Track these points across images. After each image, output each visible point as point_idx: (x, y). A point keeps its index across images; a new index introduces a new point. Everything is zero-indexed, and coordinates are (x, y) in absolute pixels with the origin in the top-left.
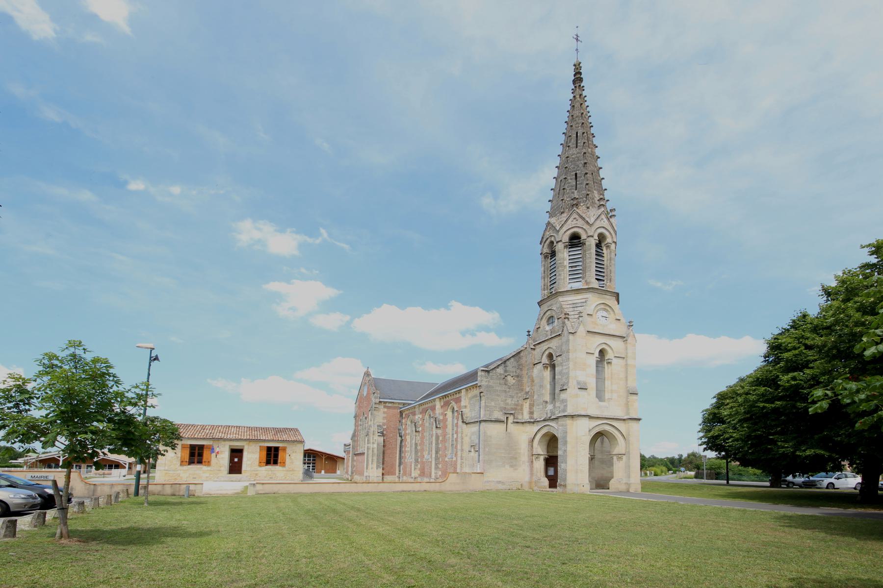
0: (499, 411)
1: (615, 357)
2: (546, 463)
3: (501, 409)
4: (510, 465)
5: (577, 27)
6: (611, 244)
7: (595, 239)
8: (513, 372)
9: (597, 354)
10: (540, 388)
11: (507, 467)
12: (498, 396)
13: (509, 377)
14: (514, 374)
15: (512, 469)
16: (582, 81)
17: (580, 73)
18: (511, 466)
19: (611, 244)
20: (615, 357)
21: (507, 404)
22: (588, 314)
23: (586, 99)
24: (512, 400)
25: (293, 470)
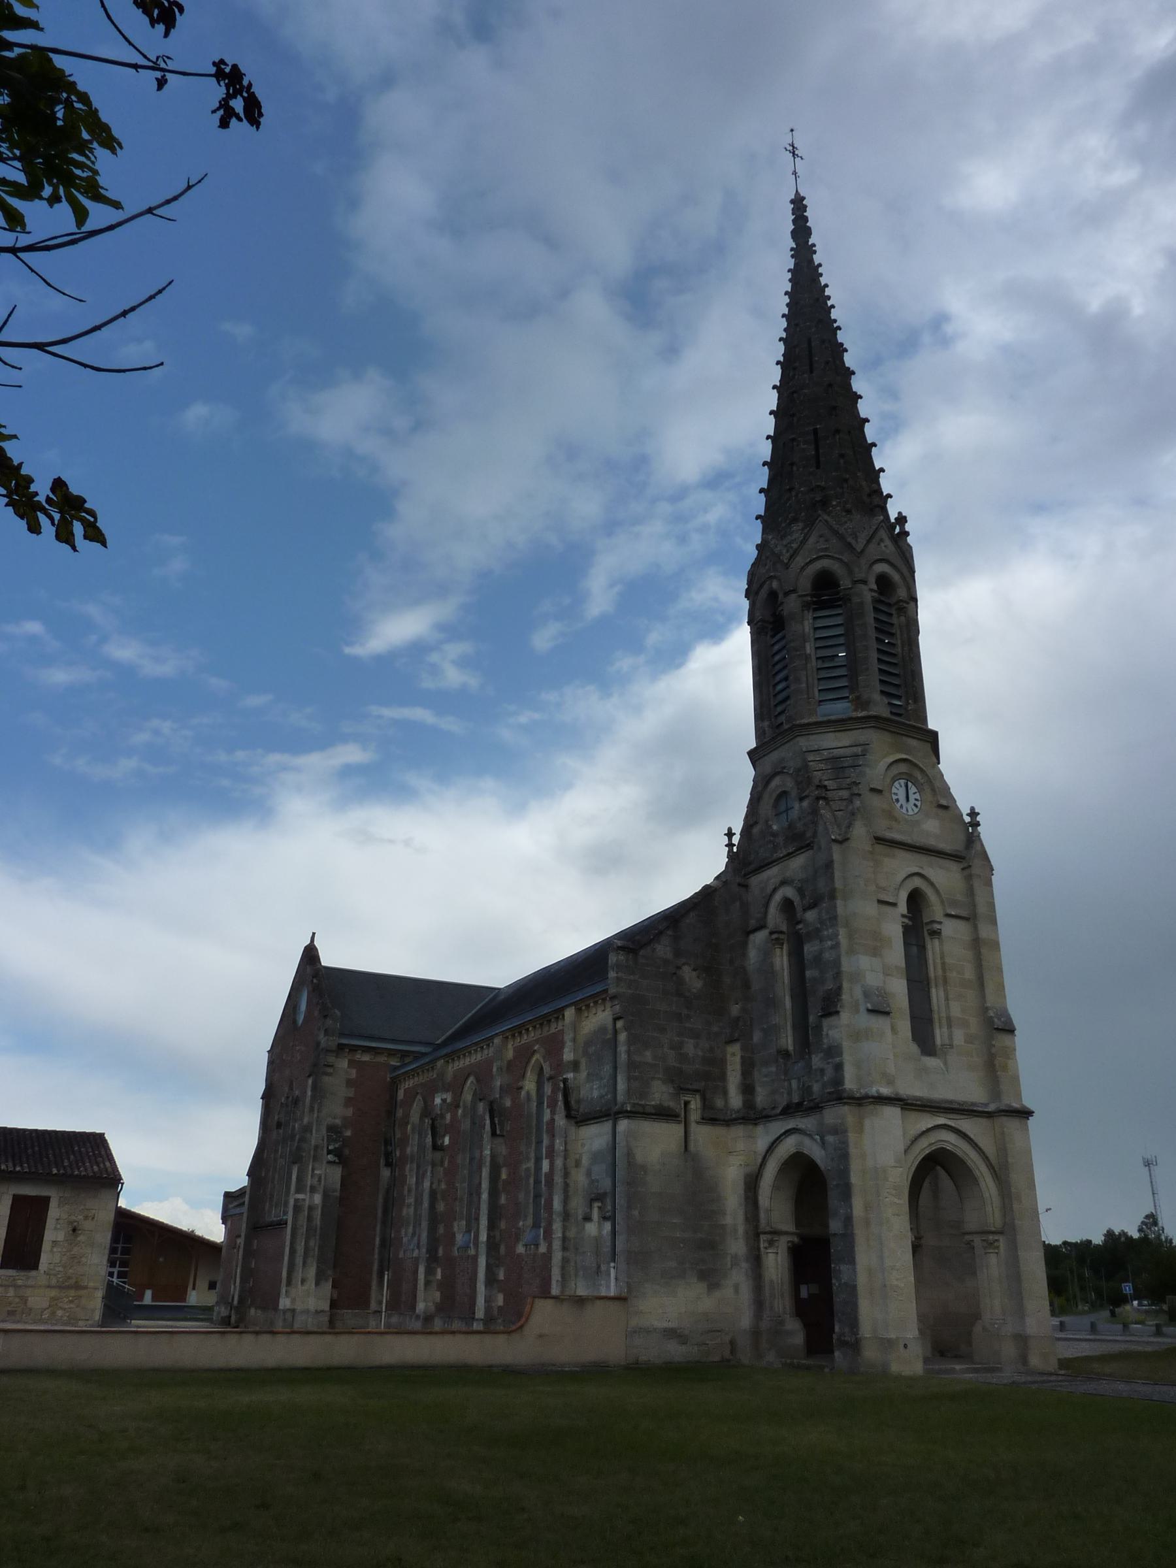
5: (792, 130)
7: (800, 596)
9: (903, 908)
25: (77, 1287)
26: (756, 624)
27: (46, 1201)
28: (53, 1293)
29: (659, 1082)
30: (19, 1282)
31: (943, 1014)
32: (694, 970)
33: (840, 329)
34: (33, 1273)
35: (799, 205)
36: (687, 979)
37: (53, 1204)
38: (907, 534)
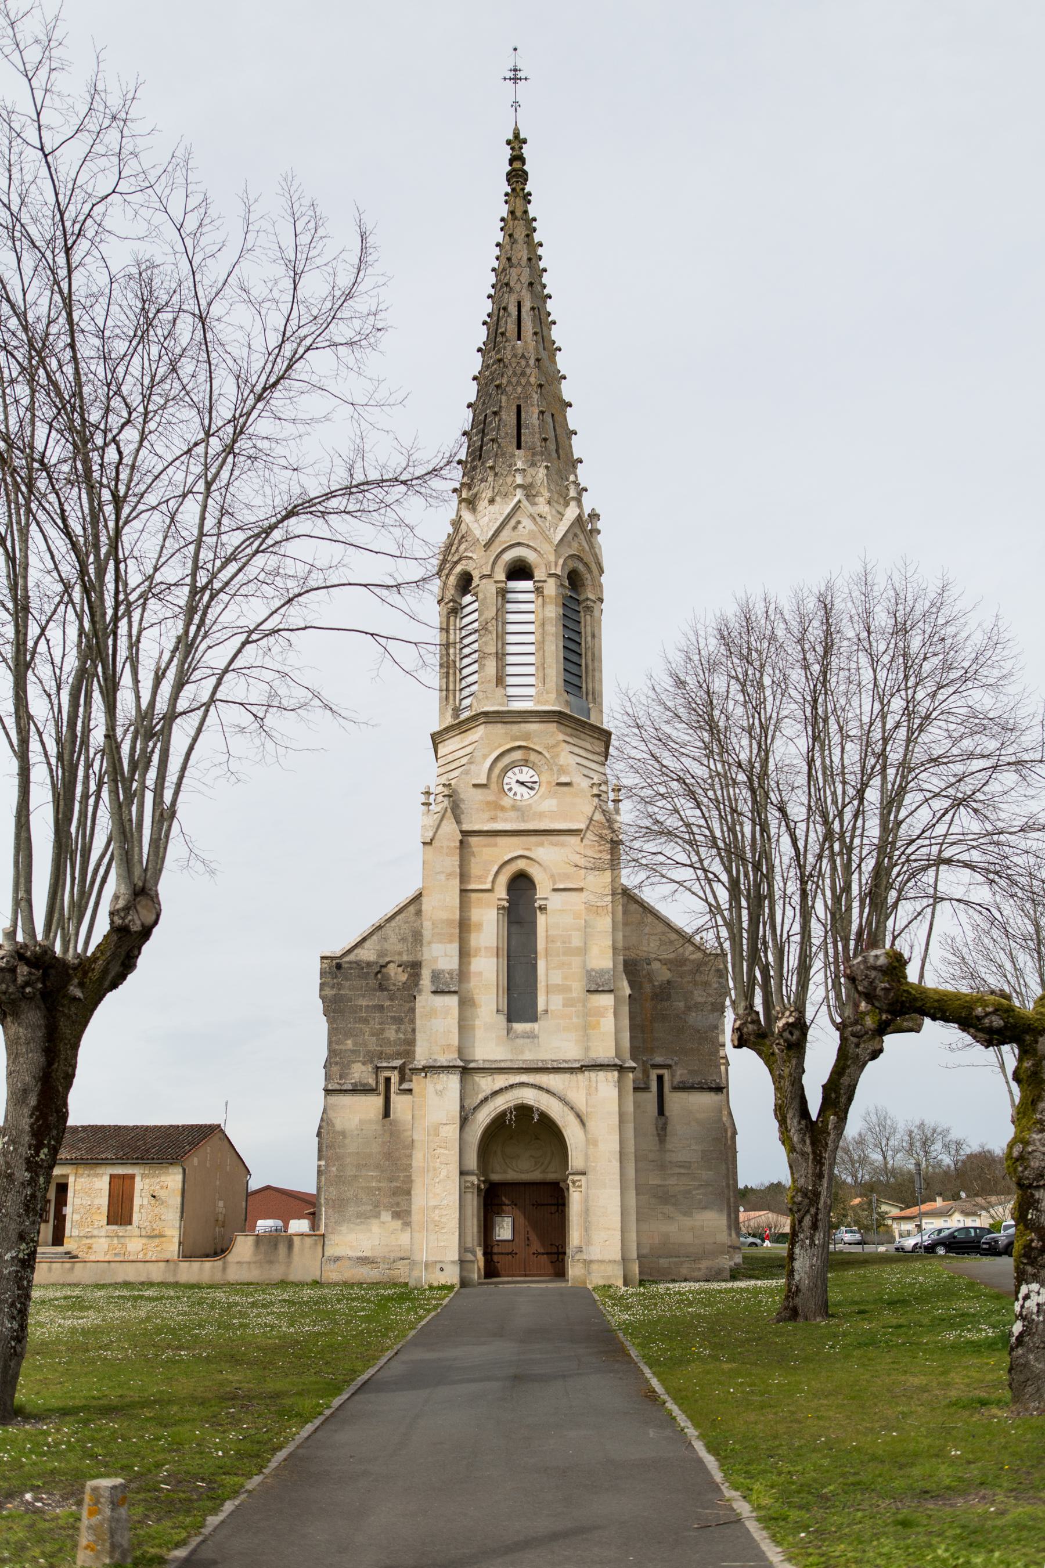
0: (364, 1064)
1: (554, 890)
2: (485, 1205)
3: (370, 1058)
4: (393, 1212)
5: (515, 49)
6: (545, 581)
7: (496, 582)
8: (400, 954)
10: (386, 989)
11: (386, 1216)
12: (366, 1021)
13: (391, 966)
14: (405, 958)
15: (400, 1222)
16: (526, 180)
17: (523, 161)
18: (396, 1215)
19: (545, 581)
20: (554, 890)
21: (388, 1042)
22: (475, 786)
23: (534, 224)
24: (397, 1031)
25: (161, 1236)
26: (447, 603)
27: (132, 1177)
28: (144, 1241)
29: (360, 1064)
30: (121, 1234)
31: (501, 960)
32: (860, 1135)
33: (550, 297)
34: (129, 1227)
35: (517, 142)
36: (392, 974)
37: (138, 1179)
38: (599, 532)
